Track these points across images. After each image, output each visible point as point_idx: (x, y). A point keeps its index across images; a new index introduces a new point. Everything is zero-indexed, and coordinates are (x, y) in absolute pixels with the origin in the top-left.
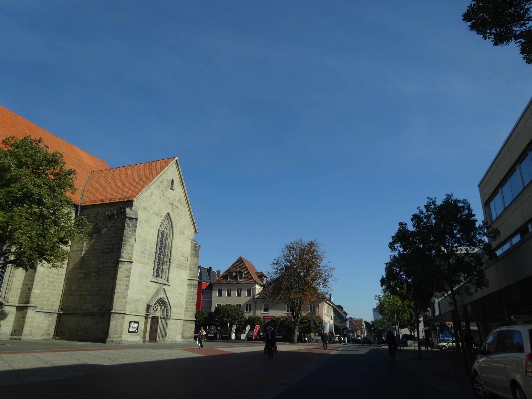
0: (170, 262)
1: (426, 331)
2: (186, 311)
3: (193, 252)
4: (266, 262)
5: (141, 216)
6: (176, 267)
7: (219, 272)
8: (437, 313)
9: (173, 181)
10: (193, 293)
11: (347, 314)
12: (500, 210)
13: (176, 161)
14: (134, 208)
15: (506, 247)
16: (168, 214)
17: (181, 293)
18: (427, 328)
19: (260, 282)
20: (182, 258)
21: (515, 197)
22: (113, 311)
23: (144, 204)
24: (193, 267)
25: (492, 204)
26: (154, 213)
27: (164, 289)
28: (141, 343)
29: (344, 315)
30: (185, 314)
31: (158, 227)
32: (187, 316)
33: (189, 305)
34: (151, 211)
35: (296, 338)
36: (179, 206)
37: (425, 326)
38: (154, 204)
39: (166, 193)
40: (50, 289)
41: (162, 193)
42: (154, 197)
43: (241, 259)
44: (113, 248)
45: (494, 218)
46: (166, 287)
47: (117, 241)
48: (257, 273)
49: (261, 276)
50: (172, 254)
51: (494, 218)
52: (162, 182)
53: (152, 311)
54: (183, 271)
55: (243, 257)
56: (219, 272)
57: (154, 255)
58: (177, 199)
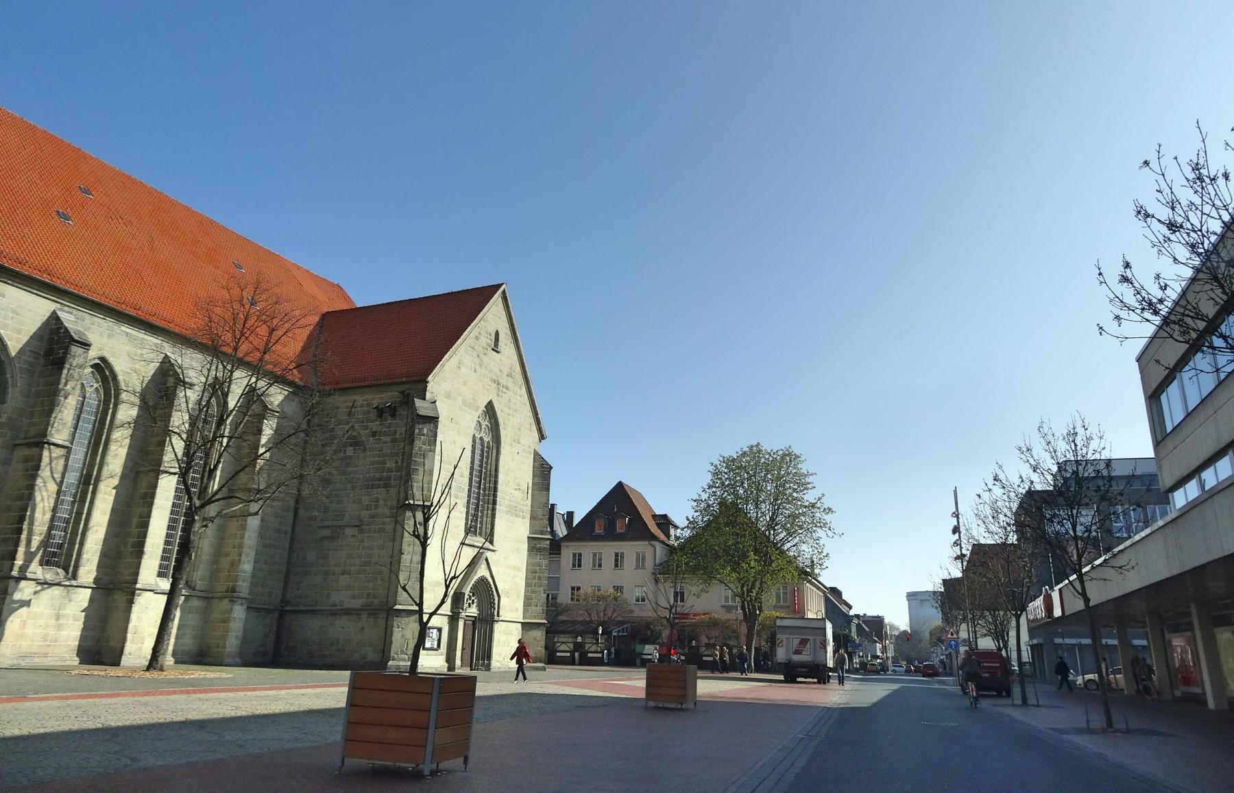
0: (494, 503)
1: (1032, 647)
2: (527, 604)
3: (537, 480)
4: (676, 496)
5: (443, 409)
6: (507, 512)
7: (570, 515)
8: (1057, 612)
9: (497, 334)
10: (540, 565)
11: (850, 607)
12: (1179, 416)
13: (504, 292)
14: (428, 396)
15: (1192, 490)
16: (490, 404)
17: (510, 565)
18: (1035, 642)
19: (662, 536)
20: (517, 493)
21: (1205, 394)
22: (138, 586)
23: (446, 386)
24: (539, 512)
25: (1163, 397)
26: (465, 403)
27: (487, 560)
28: (445, 670)
29: (844, 608)
30: (525, 611)
31: (472, 431)
32: (528, 615)
33: (534, 592)
34: (460, 399)
35: (436, 684)
36: (510, 385)
37: (1031, 638)
38: (465, 384)
39: (486, 359)
40: (266, 562)
41: (477, 361)
42: (463, 370)
43: (620, 485)
44: (389, 478)
45: (1169, 429)
46: (489, 554)
47: (397, 462)
48: (655, 516)
49: (664, 522)
50: (500, 487)
51: (1169, 429)
52: (477, 338)
53: (466, 605)
54: (520, 520)
55: (631, 482)
56: (570, 515)
57: (467, 488)
58: (506, 371)
